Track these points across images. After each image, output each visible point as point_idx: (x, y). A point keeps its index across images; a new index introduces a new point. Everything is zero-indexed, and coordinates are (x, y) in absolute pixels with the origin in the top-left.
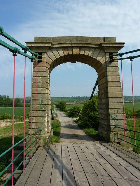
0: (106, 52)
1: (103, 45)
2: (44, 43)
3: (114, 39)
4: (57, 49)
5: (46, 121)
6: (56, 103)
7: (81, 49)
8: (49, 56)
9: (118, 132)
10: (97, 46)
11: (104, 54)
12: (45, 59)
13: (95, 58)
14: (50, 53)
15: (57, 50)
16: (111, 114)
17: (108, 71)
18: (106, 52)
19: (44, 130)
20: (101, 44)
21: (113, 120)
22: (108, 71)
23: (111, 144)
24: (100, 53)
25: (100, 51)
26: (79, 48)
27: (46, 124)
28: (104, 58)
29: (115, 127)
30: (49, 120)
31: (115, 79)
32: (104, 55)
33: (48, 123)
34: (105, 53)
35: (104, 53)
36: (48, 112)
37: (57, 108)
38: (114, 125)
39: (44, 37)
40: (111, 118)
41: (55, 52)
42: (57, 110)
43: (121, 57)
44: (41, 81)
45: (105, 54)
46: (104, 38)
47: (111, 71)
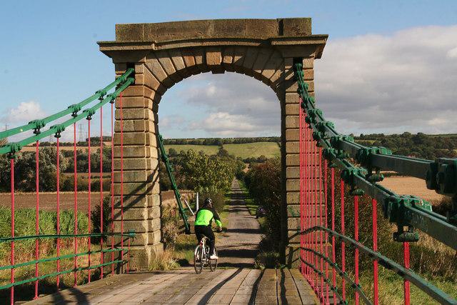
1: (274, 43)
3: (306, 22)
4: (169, 54)
5: (147, 230)
8: (149, 71)
9: (304, 246)
10: (257, 44)
12: (141, 78)
13: (260, 72)
14: (153, 63)
17: (289, 103)
19: (141, 238)
20: (270, 40)
21: (294, 217)
22: (289, 103)
26: (220, 49)
27: (145, 224)
28: (279, 73)
30: (152, 215)
34: (284, 58)
36: (148, 200)
38: (295, 228)
39: (138, 25)
40: (289, 214)
41: (165, 60)
43: (57, 136)
44: (133, 130)
45: (283, 61)
46: (281, 22)
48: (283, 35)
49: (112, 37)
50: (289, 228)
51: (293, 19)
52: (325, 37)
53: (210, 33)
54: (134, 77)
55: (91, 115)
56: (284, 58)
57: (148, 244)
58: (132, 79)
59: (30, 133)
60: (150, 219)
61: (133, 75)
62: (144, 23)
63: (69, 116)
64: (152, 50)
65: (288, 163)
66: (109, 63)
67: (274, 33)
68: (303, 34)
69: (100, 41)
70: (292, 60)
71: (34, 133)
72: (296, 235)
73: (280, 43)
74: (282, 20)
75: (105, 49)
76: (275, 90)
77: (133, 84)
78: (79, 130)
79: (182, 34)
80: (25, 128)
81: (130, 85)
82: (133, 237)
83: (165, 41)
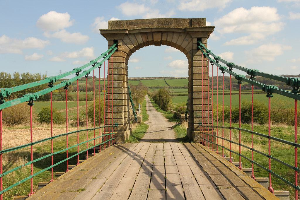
0: (192, 37)
2: (121, 30)
5: (123, 117)
6: (150, 91)
7: (163, 34)
11: (190, 40)
12: (121, 48)
15: (135, 37)
16: (195, 111)
18: (192, 37)
20: (186, 29)
23: (192, 143)
24: (186, 39)
25: (186, 35)
29: (199, 126)
31: (202, 70)
32: (191, 40)
33: (125, 120)
34: (192, 38)
35: (191, 39)
36: (124, 108)
37: (152, 103)
40: (195, 116)
42: (153, 108)
44: (117, 73)
45: (192, 39)
47: (198, 61)
48: (192, 26)
49: (30, 74)
50: (194, 122)
51: (197, 19)
52: (214, 27)
53: (155, 25)
54: (117, 47)
55: (100, 65)
56: (192, 38)
57: (126, 118)
58: (116, 48)
59: (74, 75)
60: (125, 118)
61: (117, 46)
62: (122, 20)
63: (91, 66)
64: (127, 33)
65: (194, 91)
66: (105, 42)
67: (187, 26)
68: (202, 26)
69: (101, 29)
70: (196, 39)
71: (76, 75)
72: (198, 126)
73: (191, 30)
74: (192, 19)
75: (104, 33)
76: (186, 54)
77: (117, 51)
78: (256, 130)
79: (141, 25)
80: (72, 72)
81: (116, 51)
82: (116, 127)
83: (133, 29)
